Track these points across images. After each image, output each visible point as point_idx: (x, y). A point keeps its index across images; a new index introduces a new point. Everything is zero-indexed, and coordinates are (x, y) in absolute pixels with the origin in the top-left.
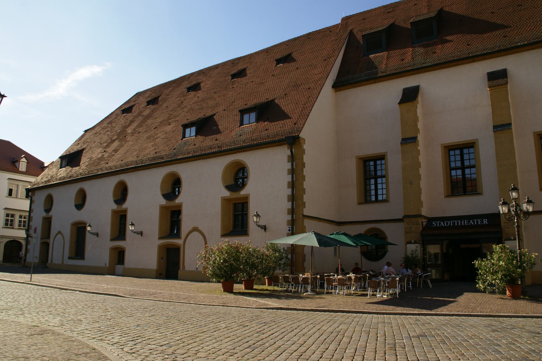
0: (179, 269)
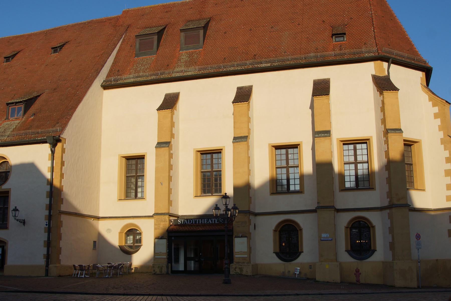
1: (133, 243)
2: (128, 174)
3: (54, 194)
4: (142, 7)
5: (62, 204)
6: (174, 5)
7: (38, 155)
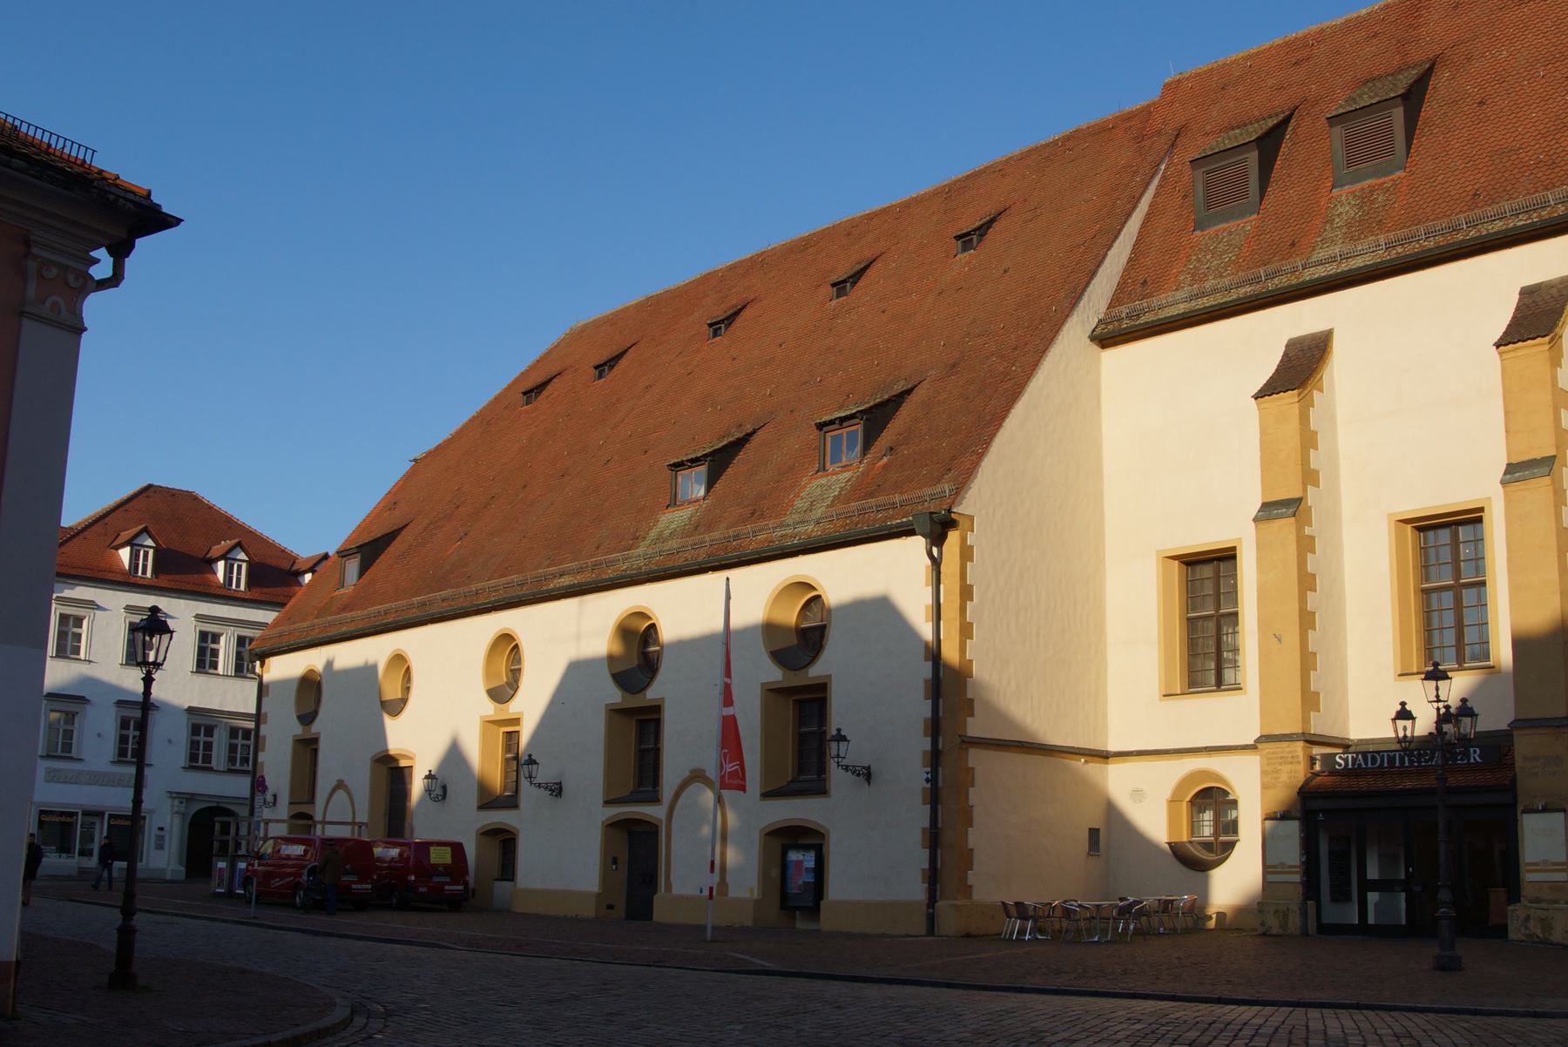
0: (655, 891)
1: (1216, 834)
2: (1194, 609)
3: (947, 686)
4: (1221, 60)
5: (972, 715)
6: (1320, 36)
7: (891, 572)
